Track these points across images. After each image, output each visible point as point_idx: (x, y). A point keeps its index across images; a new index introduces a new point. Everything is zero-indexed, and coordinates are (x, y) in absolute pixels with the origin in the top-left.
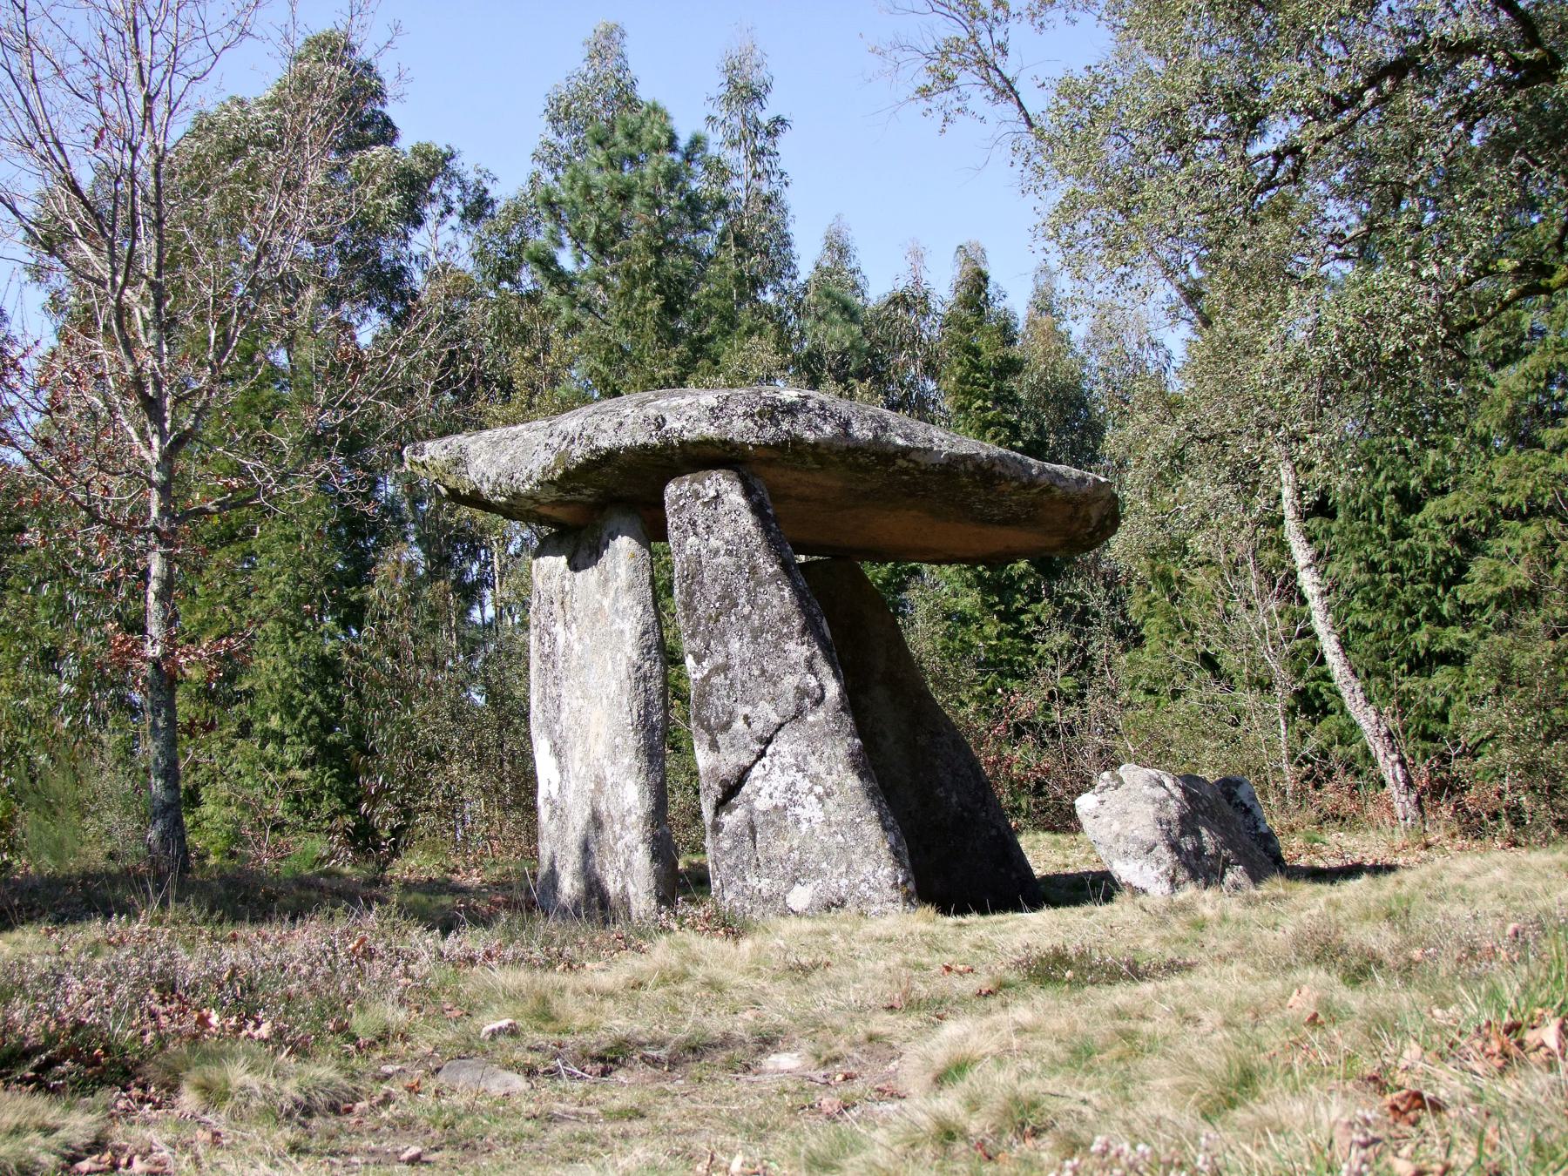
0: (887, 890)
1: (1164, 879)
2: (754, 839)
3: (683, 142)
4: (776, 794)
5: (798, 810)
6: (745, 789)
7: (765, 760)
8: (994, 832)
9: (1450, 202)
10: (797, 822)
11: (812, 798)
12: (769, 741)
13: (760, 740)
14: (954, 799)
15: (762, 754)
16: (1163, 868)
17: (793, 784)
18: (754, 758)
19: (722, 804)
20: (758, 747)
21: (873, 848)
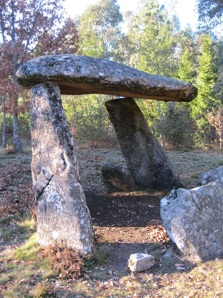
0: (78, 241)
1: (182, 242)
2: (46, 211)
3: (161, 5)
4: (51, 198)
5: (57, 205)
6: (44, 194)
7: (49, 186)
8: (168, 168)
9: (160, 44)
10: (56, 209)
11: (60, 202)
12: (50, 180)
13: (47, 179)
14: (158, 160)
15: (48, 184)
16: (183, 238)
17: (56, 196)
18: (46, 185)
19: (38, 198)
20: (47, 182)
21: (75, 225)
